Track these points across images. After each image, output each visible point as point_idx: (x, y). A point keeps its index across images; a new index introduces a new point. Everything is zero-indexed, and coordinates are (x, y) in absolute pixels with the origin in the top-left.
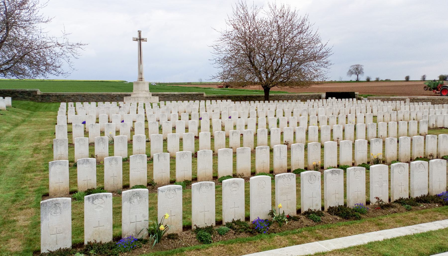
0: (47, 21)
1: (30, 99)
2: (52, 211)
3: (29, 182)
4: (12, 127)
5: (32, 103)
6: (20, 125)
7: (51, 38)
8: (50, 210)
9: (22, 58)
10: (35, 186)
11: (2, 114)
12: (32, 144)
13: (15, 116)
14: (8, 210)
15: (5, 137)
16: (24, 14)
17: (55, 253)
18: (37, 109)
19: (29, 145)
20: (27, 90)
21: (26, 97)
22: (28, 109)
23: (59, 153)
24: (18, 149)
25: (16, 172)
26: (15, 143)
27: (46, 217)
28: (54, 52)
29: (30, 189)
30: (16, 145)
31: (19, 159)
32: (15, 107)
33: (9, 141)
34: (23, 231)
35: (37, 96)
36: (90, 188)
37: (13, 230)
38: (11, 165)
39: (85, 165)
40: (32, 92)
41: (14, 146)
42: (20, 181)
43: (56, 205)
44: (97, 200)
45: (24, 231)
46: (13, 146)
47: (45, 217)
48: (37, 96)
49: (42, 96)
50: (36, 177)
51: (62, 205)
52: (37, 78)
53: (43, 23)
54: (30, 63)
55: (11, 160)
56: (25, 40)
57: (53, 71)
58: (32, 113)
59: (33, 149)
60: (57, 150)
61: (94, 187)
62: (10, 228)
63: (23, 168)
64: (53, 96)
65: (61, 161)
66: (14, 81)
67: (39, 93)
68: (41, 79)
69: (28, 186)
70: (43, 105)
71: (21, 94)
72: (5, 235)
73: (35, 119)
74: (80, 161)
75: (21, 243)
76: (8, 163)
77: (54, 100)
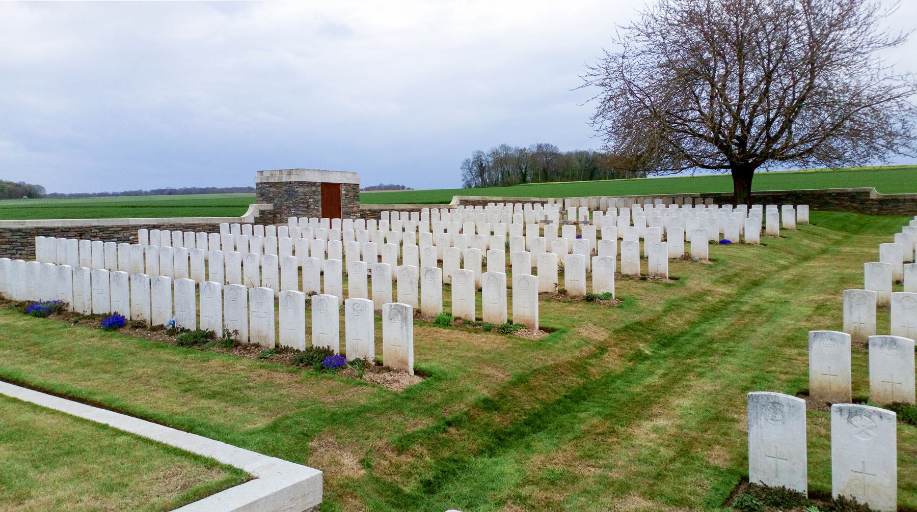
0: (895, 43)
1: (855, 208)
2: (767, 412)
3: (784, 364)
4: (795, 260)
5: (854, 216)
6: (814, 258)
7: (904, 77)
8: (764, 410)
9: (837, 126)
10: (793, 374)
11: (784, 238)
12: (816, 297)
13: (808, 242)
14: (731, 400)
15: (773, 279)
16: (846, 36)
17: (772, 491)
18: (861, 228)
19: (811, 298)
20: (849, 191)
21: (847, 204)
22: (843, 229)
23: (855, 318)
24: (788, 302)
25: (768, 342)
26: (787, 291)
27: (757, 421)
28: (907, 107)
29: (783, 377)
30: (787, 295)
31: (782, 321)
32: (815, 225)
33: (778, 286)
34: (739, 440)
35: (870, 202)
36: (898, 401)
37: (725, 434)
38: (763, 330)
39: (886, 350)
40: (860, 193)
41: (784, 296)
42: (769, 359)
43: (776, 405)
44: (858, 417)
45: (741, 441)
46: (781, 296)
47: (756, 421)
48: (870, 202)
49: (882, 202)
50: (800, 358)
51: (785, 409)
52: (868, 165)
53: (888, 49)
54: (854, 134)
55: (768, 321)
56: (846, 89)
57: (902, 150)
58: (846, 237)
59: (816, 305)
60: (851, 312)
61: (909, 402)
62: (722, 428)
63: (784, 337)
64: (905, 201)
65: (834, 334)
66: (821, 172)
67: (875, 194)
68: (874, 166)
69: (778, 369)
70: (878, 221)
71: (836, 199)
72: (710, 437)
73: (848, 249)
74: (876, 339)
75: (728, 457)
76: (760, 325)
77: (908, 209)
